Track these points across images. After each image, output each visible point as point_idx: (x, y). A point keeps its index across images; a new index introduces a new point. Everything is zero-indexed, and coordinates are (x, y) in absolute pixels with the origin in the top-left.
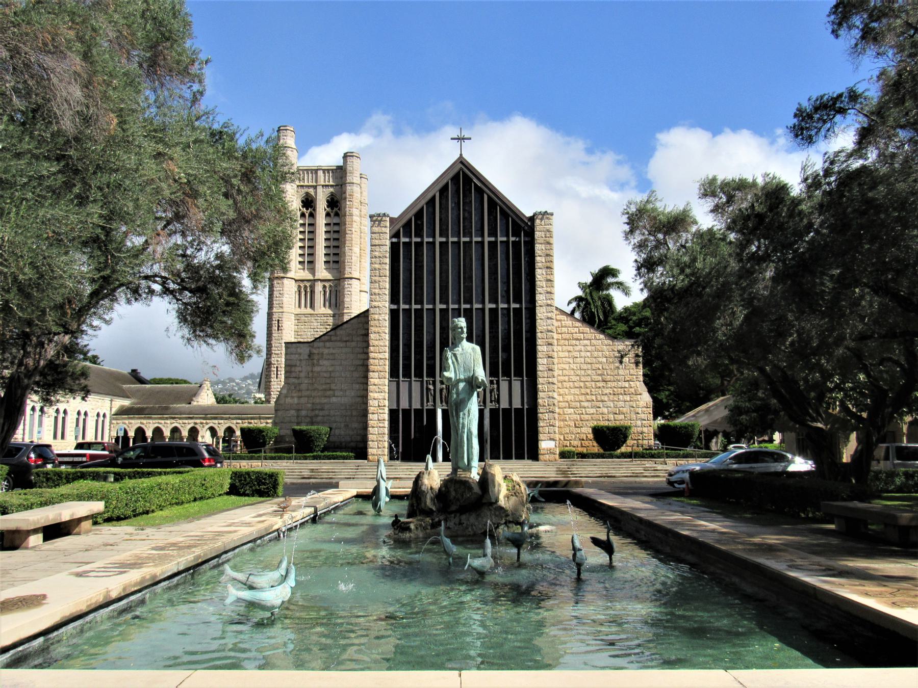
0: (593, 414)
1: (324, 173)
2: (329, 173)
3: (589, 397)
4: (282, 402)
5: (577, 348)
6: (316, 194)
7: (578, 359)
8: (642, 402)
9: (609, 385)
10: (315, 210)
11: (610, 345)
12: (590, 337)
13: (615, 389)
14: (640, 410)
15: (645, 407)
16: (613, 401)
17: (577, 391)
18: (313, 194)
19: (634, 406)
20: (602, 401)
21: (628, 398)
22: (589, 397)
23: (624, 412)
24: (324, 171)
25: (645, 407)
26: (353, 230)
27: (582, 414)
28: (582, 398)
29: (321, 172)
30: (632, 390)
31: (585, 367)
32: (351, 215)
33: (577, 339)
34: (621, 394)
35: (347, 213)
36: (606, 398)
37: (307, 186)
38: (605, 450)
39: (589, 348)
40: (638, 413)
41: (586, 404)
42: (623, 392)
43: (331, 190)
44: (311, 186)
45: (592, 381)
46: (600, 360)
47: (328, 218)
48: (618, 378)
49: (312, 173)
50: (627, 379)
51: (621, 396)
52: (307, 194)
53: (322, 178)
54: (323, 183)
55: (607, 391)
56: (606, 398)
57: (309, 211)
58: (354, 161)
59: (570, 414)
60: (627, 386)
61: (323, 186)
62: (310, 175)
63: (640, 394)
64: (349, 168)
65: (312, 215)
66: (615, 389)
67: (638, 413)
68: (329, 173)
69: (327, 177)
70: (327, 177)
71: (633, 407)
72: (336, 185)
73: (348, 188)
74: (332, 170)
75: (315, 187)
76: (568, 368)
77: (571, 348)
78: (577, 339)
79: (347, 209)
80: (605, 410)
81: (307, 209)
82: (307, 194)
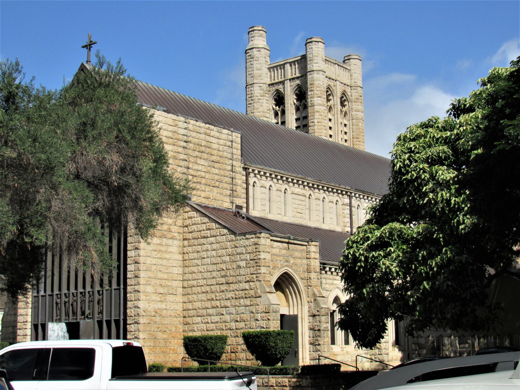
0: (217, 322)
1: (291, 66)
2: (295, 65)
3: (214, 303)
4: (5, 320)
5: (205, 247)
6: (284, 91)
7: (205, 260)
8: (261, 307)
9: (233, 287)
10: (284, 107)
11: (232, 241)
12: (214, 234)
13: (217, 294)
14: (259, 316)
15: (263, 312)
16: (235, 306)
17: (203, 297)
18: (282, 90)
19: (254, 311)
20: (226, 307)
21: (248, 302)
22: (214, 303)
23: (245, 318)
24: (290, 63)
25: (263, 312)
26: (316, 121)
27: (208, 323)
28: (208, 304)
29: (288, 65)
30: (252, 292)
31: (211, 268)
32: (313, 105)
33: (204, 237)
34: (242, 298)
35: (309, 105)
36: (228, 303)
37: (276, 83)
38: (264, 364)
39: (215, 246)
40: (257, 320)
41: (210, 311)
42: (243, 295)
43: (298, 82)
44: (280, 82)
45: (217, 284)
46: (224, 258)
47: (299, 113)
48: (240, 278)
49: (281, 69)
50: (248, 279)
51: (242, 300)
52: (278, 91)
53: (290, 71)
54: (290, 77)
55: (230, 295)
56: (228, 303)
57: (281, 108)
58: (313, 46)
59: (198, 323)
60: (247, 287)
61: (290, 80)
62: (279, 71)
63: (260, 297)
64: (308, 56)
65: (283, 112)
66: (237, 293)
67: (257, 320)
68: (295, 65)
69: (293, 70)
70: (293, 70)
71: (252, 312)
72: (301, 77)
73: (309, 77)
74: (297, 61)
75: (283, 83)
76: (196, 271)
77: (199, 248)
78: (204, 237)
79: (309, 100)
80: (228, 318)
81: (279, 107)
82: (278, 91)
